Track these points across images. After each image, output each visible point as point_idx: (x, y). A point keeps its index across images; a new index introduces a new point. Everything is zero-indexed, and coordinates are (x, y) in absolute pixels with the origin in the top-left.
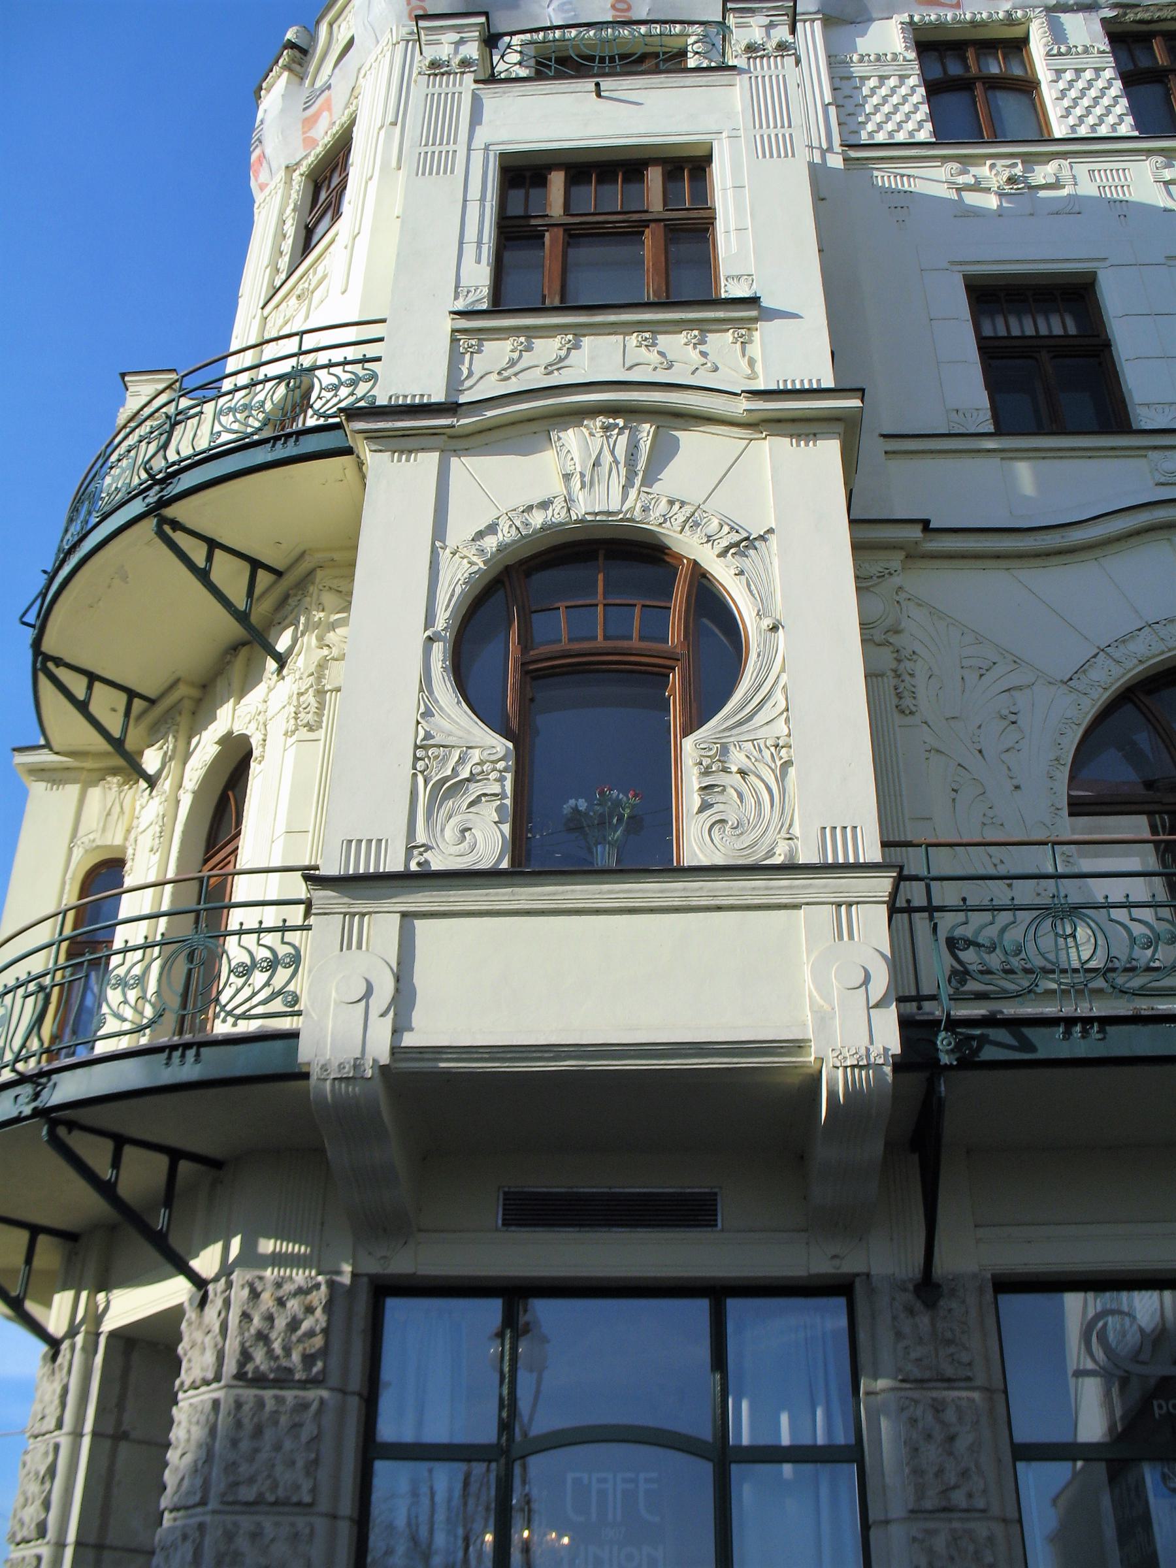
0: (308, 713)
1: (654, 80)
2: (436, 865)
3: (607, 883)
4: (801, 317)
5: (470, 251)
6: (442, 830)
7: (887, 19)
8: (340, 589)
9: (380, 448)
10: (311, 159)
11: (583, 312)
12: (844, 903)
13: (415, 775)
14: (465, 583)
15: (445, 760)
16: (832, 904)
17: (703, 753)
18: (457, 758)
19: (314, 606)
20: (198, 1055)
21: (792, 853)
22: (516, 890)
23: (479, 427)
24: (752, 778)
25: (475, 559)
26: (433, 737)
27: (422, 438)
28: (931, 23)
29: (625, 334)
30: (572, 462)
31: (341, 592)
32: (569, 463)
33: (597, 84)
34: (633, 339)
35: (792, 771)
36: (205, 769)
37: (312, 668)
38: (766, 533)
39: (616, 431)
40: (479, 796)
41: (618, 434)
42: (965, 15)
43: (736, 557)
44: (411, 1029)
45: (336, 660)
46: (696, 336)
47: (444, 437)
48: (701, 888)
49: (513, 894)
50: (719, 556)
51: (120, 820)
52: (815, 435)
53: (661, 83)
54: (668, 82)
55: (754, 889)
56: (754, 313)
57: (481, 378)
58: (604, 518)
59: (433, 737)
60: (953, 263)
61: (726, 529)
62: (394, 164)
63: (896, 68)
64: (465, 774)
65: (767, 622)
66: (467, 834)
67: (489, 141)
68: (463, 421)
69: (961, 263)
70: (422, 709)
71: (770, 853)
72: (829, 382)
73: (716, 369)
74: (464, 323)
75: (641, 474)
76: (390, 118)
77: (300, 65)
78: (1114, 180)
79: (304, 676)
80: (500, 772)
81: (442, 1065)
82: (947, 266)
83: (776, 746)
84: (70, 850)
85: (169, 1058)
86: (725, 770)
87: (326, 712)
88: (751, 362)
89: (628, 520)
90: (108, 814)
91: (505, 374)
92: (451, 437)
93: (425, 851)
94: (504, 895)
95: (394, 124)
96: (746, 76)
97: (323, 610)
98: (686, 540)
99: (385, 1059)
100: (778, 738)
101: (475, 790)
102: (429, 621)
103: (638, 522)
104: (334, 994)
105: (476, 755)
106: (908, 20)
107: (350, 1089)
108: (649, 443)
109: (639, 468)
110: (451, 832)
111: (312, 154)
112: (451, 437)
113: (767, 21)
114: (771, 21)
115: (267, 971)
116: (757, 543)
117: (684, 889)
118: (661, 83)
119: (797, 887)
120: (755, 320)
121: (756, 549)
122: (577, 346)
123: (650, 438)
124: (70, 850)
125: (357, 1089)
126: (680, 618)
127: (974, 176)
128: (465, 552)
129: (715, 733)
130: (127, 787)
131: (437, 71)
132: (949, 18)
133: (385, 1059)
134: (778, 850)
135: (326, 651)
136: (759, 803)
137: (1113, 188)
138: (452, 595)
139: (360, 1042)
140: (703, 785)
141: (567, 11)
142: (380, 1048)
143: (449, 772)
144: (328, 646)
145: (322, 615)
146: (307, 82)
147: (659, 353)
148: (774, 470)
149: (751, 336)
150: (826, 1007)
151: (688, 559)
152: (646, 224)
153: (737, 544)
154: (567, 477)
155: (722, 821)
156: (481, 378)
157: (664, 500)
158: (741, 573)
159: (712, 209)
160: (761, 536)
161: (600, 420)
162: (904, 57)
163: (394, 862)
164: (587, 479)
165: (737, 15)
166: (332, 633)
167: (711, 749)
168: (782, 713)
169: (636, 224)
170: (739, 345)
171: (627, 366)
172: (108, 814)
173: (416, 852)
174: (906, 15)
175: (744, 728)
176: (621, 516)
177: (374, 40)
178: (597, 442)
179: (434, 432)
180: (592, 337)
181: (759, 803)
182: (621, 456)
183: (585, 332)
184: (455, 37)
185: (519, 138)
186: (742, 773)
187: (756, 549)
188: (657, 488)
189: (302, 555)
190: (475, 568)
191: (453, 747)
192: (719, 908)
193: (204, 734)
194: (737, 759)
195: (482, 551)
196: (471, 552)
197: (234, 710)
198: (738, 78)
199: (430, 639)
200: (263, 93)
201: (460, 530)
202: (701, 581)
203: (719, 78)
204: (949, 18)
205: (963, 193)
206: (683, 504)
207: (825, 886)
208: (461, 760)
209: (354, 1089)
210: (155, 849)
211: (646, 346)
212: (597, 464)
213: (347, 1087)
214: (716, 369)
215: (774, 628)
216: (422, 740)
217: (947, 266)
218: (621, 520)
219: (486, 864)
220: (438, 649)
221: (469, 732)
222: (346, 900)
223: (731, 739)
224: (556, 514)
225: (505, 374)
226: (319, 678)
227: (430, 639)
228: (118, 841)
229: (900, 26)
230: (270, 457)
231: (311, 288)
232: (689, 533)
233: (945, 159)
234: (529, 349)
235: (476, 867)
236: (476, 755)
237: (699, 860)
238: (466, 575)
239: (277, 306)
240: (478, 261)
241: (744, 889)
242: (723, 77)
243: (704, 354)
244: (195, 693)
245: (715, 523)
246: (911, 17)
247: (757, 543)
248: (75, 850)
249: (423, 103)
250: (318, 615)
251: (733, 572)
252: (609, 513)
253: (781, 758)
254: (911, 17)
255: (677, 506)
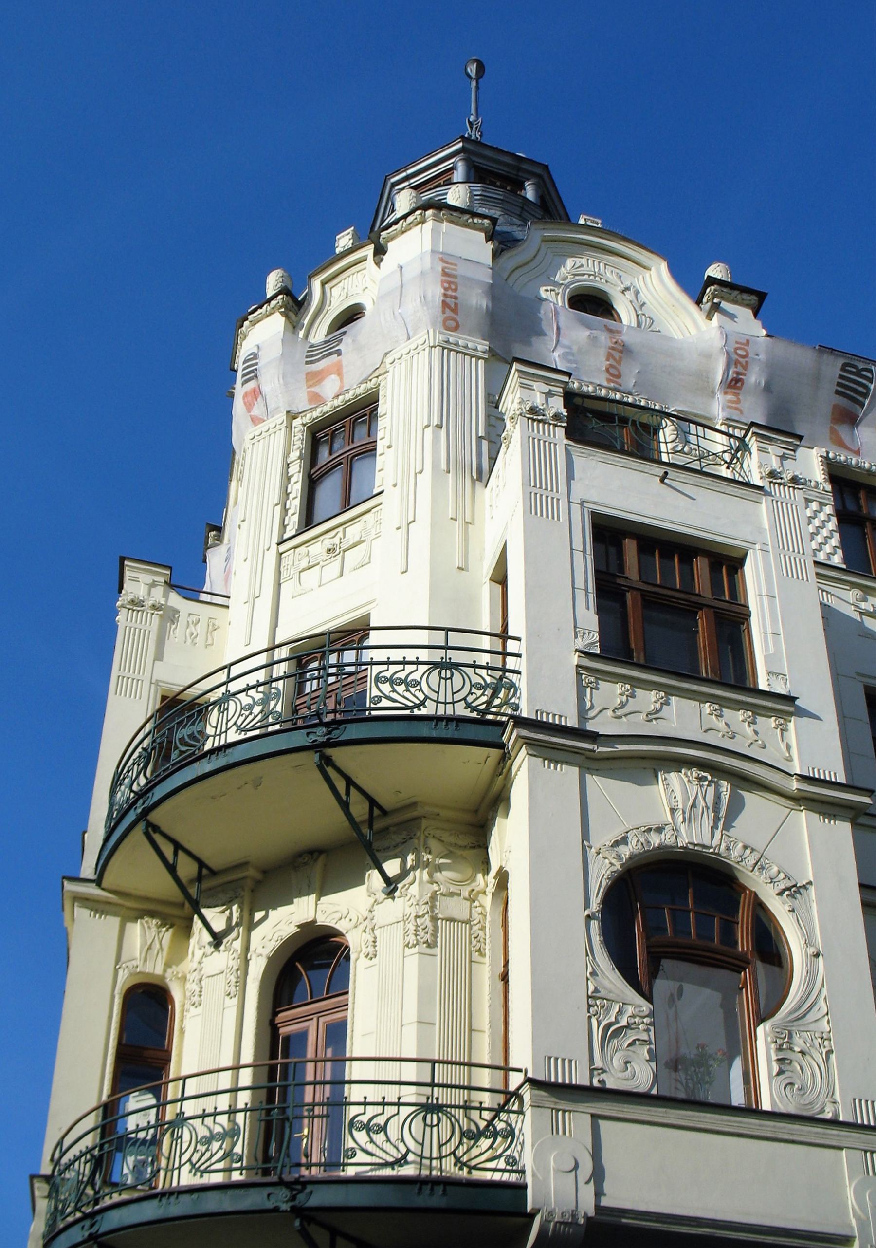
0: (427, 933)
1: (703, 481)
2: (610, 1085)
3: (728, 1115)
4: (820, 719)
5: (580, 595)
6: (612, 1060)
7: (809, 448)
8: (442, 839)
9: (535, 753)
10: (316, 414)
11: (673, 677)
12: (869, 1151)
13: (590, 1017)
14: (608, 878)
15: (608, 1011)
16: (862, 1150)
17: (777, 1035)
18: (617, 1010)
19: (422, 849)
20: (444, 1190)
21: (836, 1114)
22: (668, 1110)
23: (612, 755)
24: (808, 1057)
25: (614, 861)
26: (599, 992)
27: (567, 753)
28: (840, 462)
29: (701, 702)
30: (675, 800)
31: (442, 841)
32: (673, 800)
33: (666, 473)
34: (707, 707)
35: (833, 1057)
36: (279, 943)
37: (426, 898)
38: (808, 883)
39: (706, 783)
40: (634, 1041)
41: (708, 786)
42: (864, 463)
43: (789, 897)
44: (605, 1195)
45: (444, 895)
46: (750, 717)
47: (583, 757)
48: (784, 1128)
49: (666, 1112)
50: (777, 894)
51: (160, 955)
52: (834, 816)
53: (708, 484)
54: (713, 486)
55: (817, 1133)
56: (792, 709)
57: (601, 711)
58: (700, 849)
59: (599, 992)
60: (858, 674)
61: (782, 876)
62: (444, 466)
63: (817, 494)
64: (624, 1023)
65: (811, 950)
66: (628, 1065)
67: (585, 498)
68: (601, 749)
69: (863, 675)
70: (590, 970)
71: (822, 1111)
72: (842, 779)
73: (764, 747)
74: (587, 662)
75: (723, 820)
76: (435, 421)
77: (296, 314)
78: (549, 435)
79: (421, 903)
80: (647, 1024)
81: (624, 1221)
82: (854, 675)
83: (822, 1038)
84: (116, 971)
85: (420, 1189)
86: (791, 1049)
87: (439, 935)
88: (788, 747)
89: (716, 854)
90: (150, 948)
91: (619, 713)
92: (588, 758)
93: (602, 1073)
94: (660, 1112)
95: (440, 427)
96: (770, 498)
97: (430, 853)
98: (754, 877)
99: (591, 1213)
100: (823, 1033)
101: (631, 1036)
102: (587, 905)
103: (722, 857)
104: (552, 1163)
105: (630, 1010)
106: (825, 455)
107: (567, 1229)
108: (727, 797)
109: (721, 815)
110: (617, 1062)
111: (319, 410)
112: (588, 758)
113: (781, 452)
114: (784, 454)
115: (489, 1138)
116: (801, 890)
117: (774, 1127)
118: (708, 484)
119: (842, 1136)
120: (791, 714)
121: (801, 894)
122: (667, 703)
123: (728, 793)
124: (116, 971)
125: (571, 1230)
126: (747, 933)
127: (872, 605)
128: (607, 854)
129: (784, 1023)
130: (164, 929)
131: (535, 417)
132: (853, 462)
133: (591, 1213)
134: (827, 1109)
135: (435, 887)
136: (813, 1075)
137: (547, 444)
138: (600, 886)
139: (575, 1199)
140: (780, 1057)
141: (570, 361)
142: (587, 1205)
143: (613, 1019)
144: (437, 883)
145: (430, 857)
146: (301, 334)
147: (726, 724)
148: (810, 836)
149: (787, 726)
150: (863, 1216)
151: (751, 891)
152: (701, 606)
153: (789, 889)
154: (673, 811)
155: (792, 1084)
156: (601, 711)
157: (740, 845)
158: (793, 910)
159: (746, 606)
160: (804, 885)
161: (695, 772)
162: (824, 487)
163: (581, 1078)
164: (687, 815)
165: (758, 439)
166: (438, 874)
167: (782, 1033)
168: (824, 1016)
169: (692, 604)
170: (778, 731)
171: (704, 728)
172: (150, 948)
173: (595, 1072)
174: (824, 450)
175: (800, 1022)
176: (711, 850)
177: (406, 337)
178: (694, 789)
179: (577, 751)
180: (678, 698)
181: (813, 1075)
182: (710, 804)
183: (674, 693)
184: (546, 388)
185: (605, 501)
186: (802, 1052)
187: (801, 894)
188: (732, 832)
189: (414, 805)
190: (615, 869)
191: (613, 1001)
192: (793, 1142)
193: (272, 913)
194: (799, 1043)
195: (619, 857)
196: (611, 856)
197: (317, 905)
198: (764, 498)
199: (589, 918)
200: (246, 323)
201: (601, 838)
202: (759, 906)
203: (750, 493)
204: (853, 462)
205: (863, 617)
206: (753, 850)
207: (859, 1138)
208: (620, 1012)
209: (569, 1230)
210: (232, 995)
211: (716, 715)
212: (694, 805)
213: (564, 1229)
214: (764, 747)
215: (817, 955)
216: (593, 993)
217: (854, 675)
218: (712, 853)
219: (643, 1089)
220: (595, 925)
221: (623, 993)
222: (553, 1099)
223: (793, 1028)
224: (666, 838)
225: (619, 713)
226: (433, 907)
227: (588, 916)
228: (159, 971)
229: (820, 459)
230: (434, 734)
231: (344, 547)
232: (757, 873)
233: (854, 585)
234: (633, 696)
235: (635, 1090)
236: (630, 1010)
237: (779, 1108)
238: (609, 872)
239: (295, 547)
240: (588, 608)
241: (809, 1132)
242: (753, 494)
243: (756, 733)
244: (258, 876)
245: (775, 869)
246: (828, 453)
247: (801, 890)
248: (121, 972)
249: (527, 444)
250: (427, 857)
251: (788, 908)
252: (704, 846)
253: (825, 1047)
254: (828, 453)
255: (748, 851)
